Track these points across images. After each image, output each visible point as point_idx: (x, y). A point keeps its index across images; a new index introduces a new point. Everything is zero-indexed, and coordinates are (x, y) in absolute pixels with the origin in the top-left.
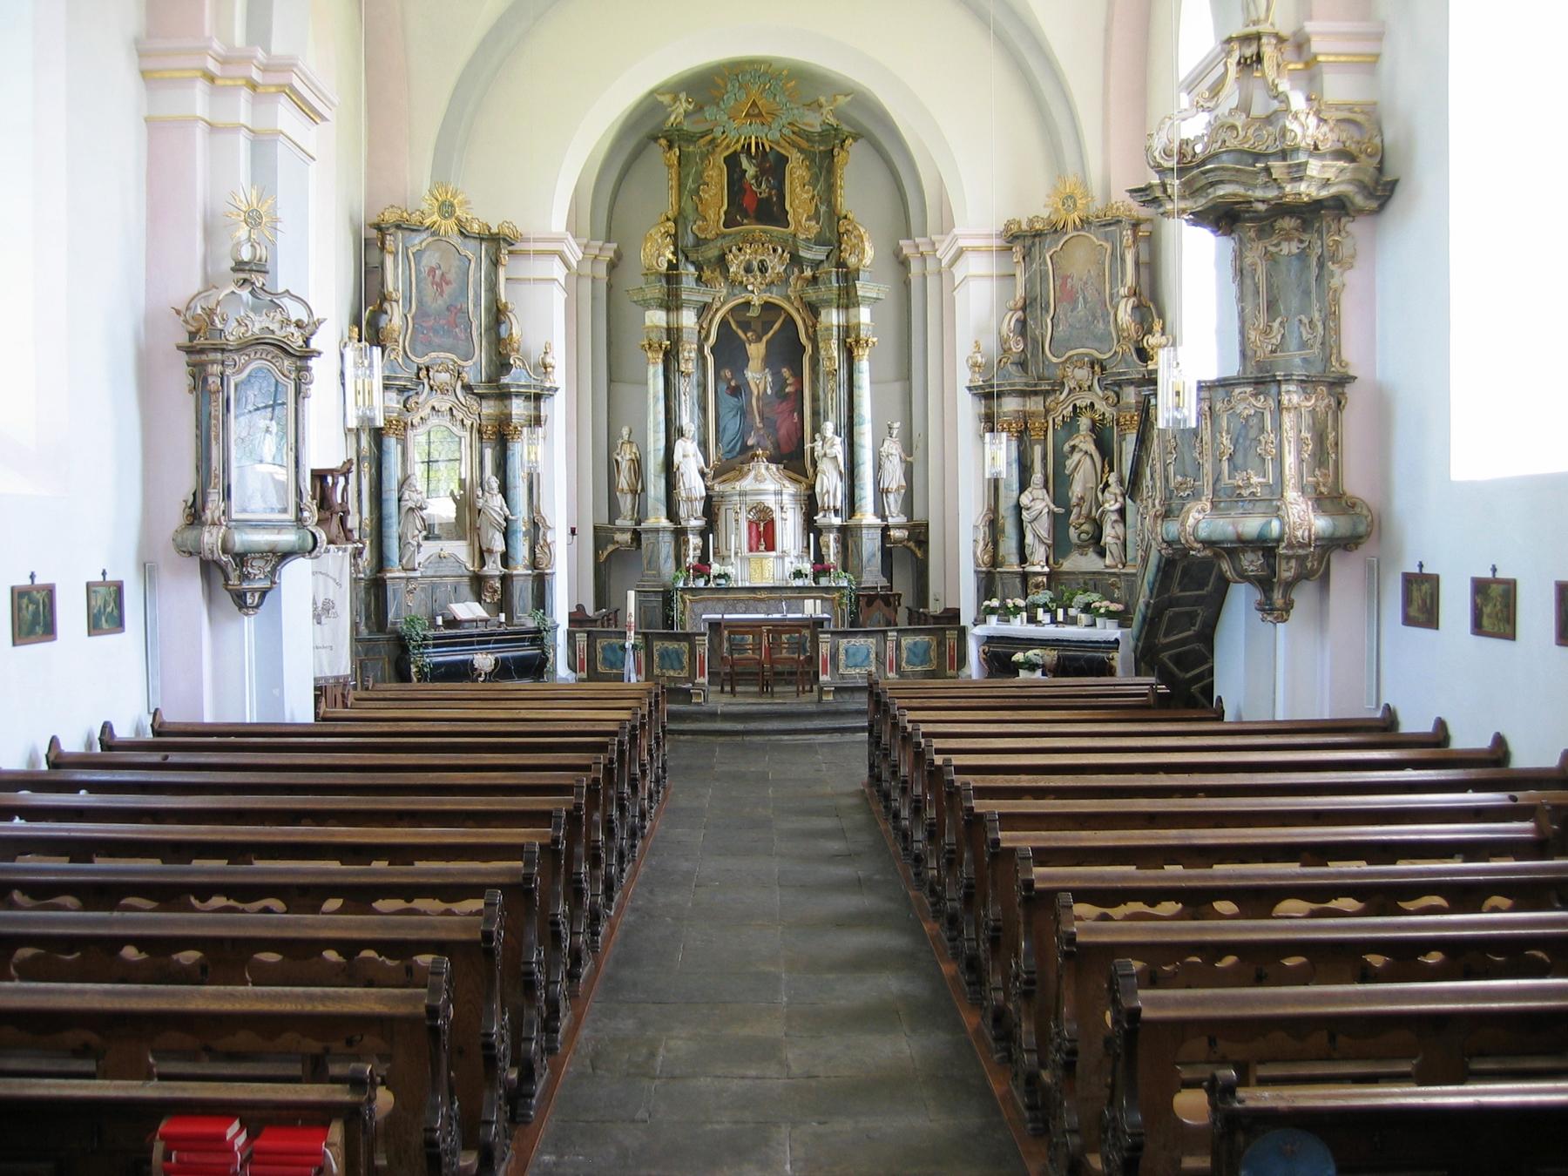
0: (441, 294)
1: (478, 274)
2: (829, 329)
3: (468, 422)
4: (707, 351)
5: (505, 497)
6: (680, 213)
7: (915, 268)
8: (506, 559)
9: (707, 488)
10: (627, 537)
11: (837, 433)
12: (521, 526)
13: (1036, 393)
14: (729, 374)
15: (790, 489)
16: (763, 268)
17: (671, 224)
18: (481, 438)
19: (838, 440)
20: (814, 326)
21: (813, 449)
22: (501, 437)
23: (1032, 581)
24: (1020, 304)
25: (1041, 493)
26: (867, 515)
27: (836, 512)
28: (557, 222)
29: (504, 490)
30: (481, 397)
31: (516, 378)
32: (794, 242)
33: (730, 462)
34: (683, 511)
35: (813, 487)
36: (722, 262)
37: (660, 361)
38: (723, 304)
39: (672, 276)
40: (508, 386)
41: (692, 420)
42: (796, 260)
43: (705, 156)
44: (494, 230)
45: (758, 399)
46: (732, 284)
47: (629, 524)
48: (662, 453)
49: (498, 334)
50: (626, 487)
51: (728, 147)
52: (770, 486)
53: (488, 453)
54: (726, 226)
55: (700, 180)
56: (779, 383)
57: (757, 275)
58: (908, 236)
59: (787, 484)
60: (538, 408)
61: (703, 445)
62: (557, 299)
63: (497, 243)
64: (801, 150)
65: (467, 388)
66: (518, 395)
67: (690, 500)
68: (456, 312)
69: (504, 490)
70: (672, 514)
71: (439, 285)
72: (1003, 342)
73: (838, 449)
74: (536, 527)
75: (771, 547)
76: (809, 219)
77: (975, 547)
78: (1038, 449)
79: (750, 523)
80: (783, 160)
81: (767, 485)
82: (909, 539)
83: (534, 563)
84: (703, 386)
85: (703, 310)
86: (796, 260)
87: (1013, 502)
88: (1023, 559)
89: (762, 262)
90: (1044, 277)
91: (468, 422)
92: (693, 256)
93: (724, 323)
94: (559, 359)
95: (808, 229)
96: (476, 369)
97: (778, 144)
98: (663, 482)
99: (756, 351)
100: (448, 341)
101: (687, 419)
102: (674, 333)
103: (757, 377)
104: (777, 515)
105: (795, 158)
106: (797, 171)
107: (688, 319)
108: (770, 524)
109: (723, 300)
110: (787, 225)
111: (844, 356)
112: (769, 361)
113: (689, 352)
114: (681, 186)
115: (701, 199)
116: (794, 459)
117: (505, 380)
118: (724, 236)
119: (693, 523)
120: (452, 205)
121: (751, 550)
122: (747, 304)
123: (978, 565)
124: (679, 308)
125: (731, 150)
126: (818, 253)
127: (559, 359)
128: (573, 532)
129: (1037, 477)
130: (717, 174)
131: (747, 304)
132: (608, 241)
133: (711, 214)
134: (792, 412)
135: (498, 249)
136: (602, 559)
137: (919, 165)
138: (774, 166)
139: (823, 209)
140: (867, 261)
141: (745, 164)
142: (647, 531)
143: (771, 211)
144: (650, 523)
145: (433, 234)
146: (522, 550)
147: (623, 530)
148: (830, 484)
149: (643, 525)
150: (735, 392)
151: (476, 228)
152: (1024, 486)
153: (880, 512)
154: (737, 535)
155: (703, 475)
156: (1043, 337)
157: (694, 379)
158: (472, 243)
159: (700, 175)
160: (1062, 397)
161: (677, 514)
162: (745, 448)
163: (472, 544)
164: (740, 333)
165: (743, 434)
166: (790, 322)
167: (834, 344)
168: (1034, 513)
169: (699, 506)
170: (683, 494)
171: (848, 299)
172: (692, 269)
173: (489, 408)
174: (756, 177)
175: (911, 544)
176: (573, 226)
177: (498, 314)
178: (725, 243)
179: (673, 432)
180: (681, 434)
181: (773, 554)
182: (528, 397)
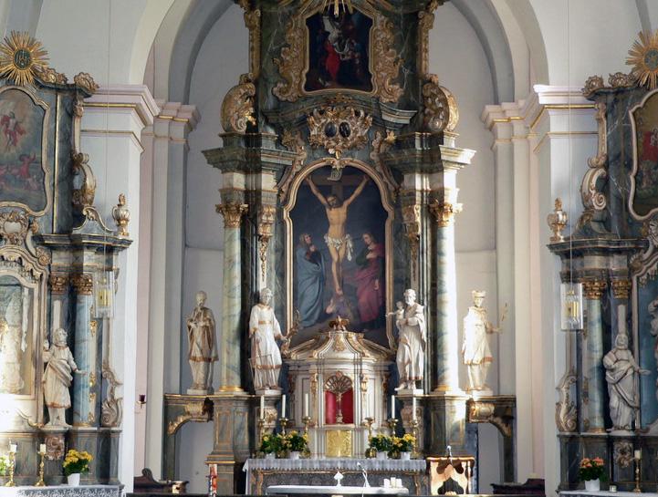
0: (14, 143)
1: (52, 124)
2: (412, 194)
3: (37, 274)
4: (286, 215)
5: (73, 350)
6: (261, 75)
7: (502, 131)
8: (71, 414)
9: (283, 357)
10: (198, 408)
11: (419, 301)
12: (88, 381)
13: (619, 252)
14: (308, 240)
15: (370, 359)
16: (345, 132)
17: (251, 85)
18: (50, 291)
19: (420, 308)
20: (397, 191)
21: (394, 318)
22: (72, 287)
23: (616, 446)
24: (602, 161)
25: (625, 354)
26: (451, 385)
27: (418, 384)
28: (135, 76)
29: (72, 343)
30: (52, 248)
31: (87, 229)
32: (378, 105)
33: (308, 332)
34: (258, 381)
35: (393, 358)
36: (303, 125)
37: (237, 224)
38: (304, 168)
39: (252, 137)
40: (80, 237)
41: (269, 285)
42: (379, 124)
43: (287, 17)
44: (71, 81)
45: (338, 264)
46: (313, 147)
47: (200, 393)
48: (237, 319)
49: (71, 185)
50: (198, 355)
51: (310, 10)
52: (350, 355)
53: (57, 305)
54: (307, 88)
55: (282, 42)
56: (361, 250)
57: (344, 139)
58: (497, 102)
59: (367, 353)
60: (109, 262)
61: (280, 313)
62: (133, 154)
63: (74, 94)
64: (385, 13)
65: (38, 239)
66: (90, 246)
67: (265, 368)
68: (29, 163)
69: (72, 343)
70: (247, 384)
71: (12, 134)
72: (585, 199)
73: (421, 318)
74: (104, 377)
75: (349, 418)
76: (393, 82)
77: (558, 410)
78: (622, 310)
79: (328, 393)
80: (367, 22)
81: (349, 357)
82: (495, 415)
83: (100, 418)
84: (281, 251)
85: (283, 172)
86: (379, 124)
87: (596, 362)
88: (608, 423)
89: (343, 124)
90: (627, 134)
91: (37, 274)
92: (273, 119)
93: (304, 187)
94: (132, 211)
95: (391, 93)
96: (48, 219)
97: (362, 7)
98: (237, 351)
99: (337, 216)
100: (20, 191)
101: (264, 283)
102: (253, 196)
103: (337, 242)
104: (356, 386)
105: (379, 20)
106: (381, 34)
107: (268, 182)
108: (349, 395)
109: (303, 162)
110: (370, 88)
111: (427, 223)
112: (349, 226)
113: (268, 215)
114: (262, 47)
115: (282, 61)
116: (377, 330)
117: (77, 231)
118: (306, 98)
119: (269, 392)
120: (28, 55)
121: (327, 422)
122: (328, 168)
123: (561, 429)
124: (258, 171)
125: (313, 13)
126: (403, 118)
127: (132, 211)
128: (142, 398)
129: (621, 338)
130: (298, 37)
131: (328, 168)
132: (186, 102)
133: (293, 75)
134: (374, 278)
135: (75, 100)
136: (172, 429)
137: (516, 263)
138: (357, 28)
139: (407, 72)
140: (451, 125)
141: (328, 26)
142: (219, 400)
143: (355, 74)
144: (221, 393)
145: (8, 83)
146: (88, 407)
147: (194, 401)
148: (413, 354)
149: (216, 395)
150: (315, 257)
151: (52, 78)
152: (607, 347)
153: (464, 384)
154: (314, 403)
155: (278, 339)
156: (627, 195)
157: (272, 243)
158: (48, 95)
159: (282, 36)
160: (646, 256)
161: (252, 383)
162: (324, 316)
163: (36, 399)
164: (321, 197)
165: (322, 300)
166: (372, 185)
167: (417, 209)
168: (618, 375)
169: (275, 376)
170: (258, 362)
171: (433, 165)
172: (271, 132)
173: (61, 260)
174: (339, 40)
175: (498, 420)
176: (151, 79)
177: (73, 164)
178: (305, 106)
179: (250, 298)
180: (257, 299)
181: (352, 426)
182: (99, 250)
